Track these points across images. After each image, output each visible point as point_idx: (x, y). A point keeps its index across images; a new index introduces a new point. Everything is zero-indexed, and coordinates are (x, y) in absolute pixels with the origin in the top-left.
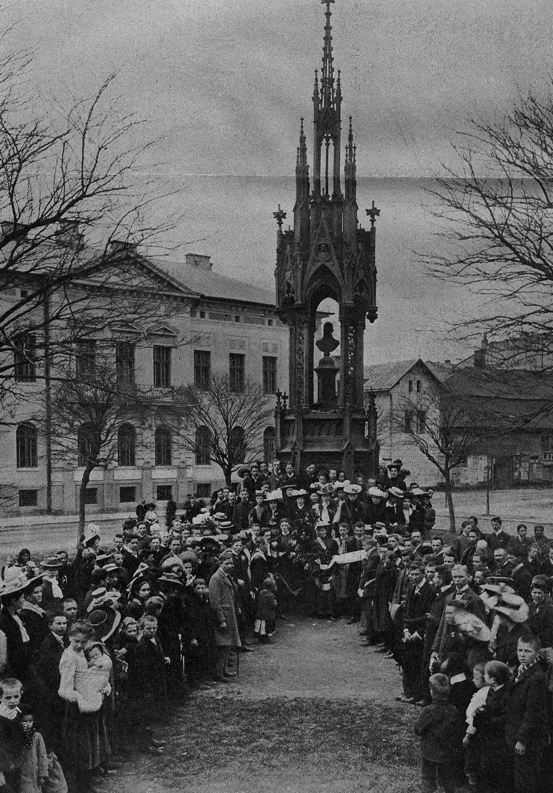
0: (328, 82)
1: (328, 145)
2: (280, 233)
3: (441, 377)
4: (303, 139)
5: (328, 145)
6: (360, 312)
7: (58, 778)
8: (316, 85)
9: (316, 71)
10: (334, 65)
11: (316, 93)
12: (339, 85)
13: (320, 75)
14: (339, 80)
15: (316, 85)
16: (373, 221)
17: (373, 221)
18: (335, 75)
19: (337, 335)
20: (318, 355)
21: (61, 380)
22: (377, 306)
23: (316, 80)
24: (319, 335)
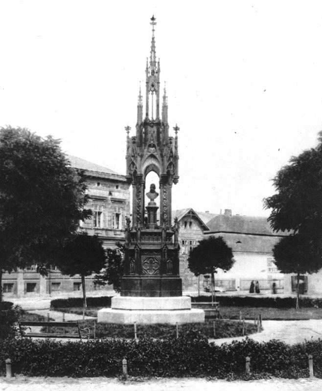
0: (153, 63)
1: (143, 244)
2: (128, 137)
3: (205, 221)
4: (140, 97)
5: (143, 244)
6: (169, 178)
7: (277, 232)
8: (147, 65)
9: (147, 58)
10: (156, 55)
11: (147, 69)
12: (159, 65)
13: (149, 60)
14: (159, 63)
15: (147, 65)
16: (176, 133)
17: (176, 133)
18: (157, 60)
19: (158, 190)
20: (147, 201)
21: (52, 279)
22: (179, 175)
23: (147, 62)
24: (148, 190)
